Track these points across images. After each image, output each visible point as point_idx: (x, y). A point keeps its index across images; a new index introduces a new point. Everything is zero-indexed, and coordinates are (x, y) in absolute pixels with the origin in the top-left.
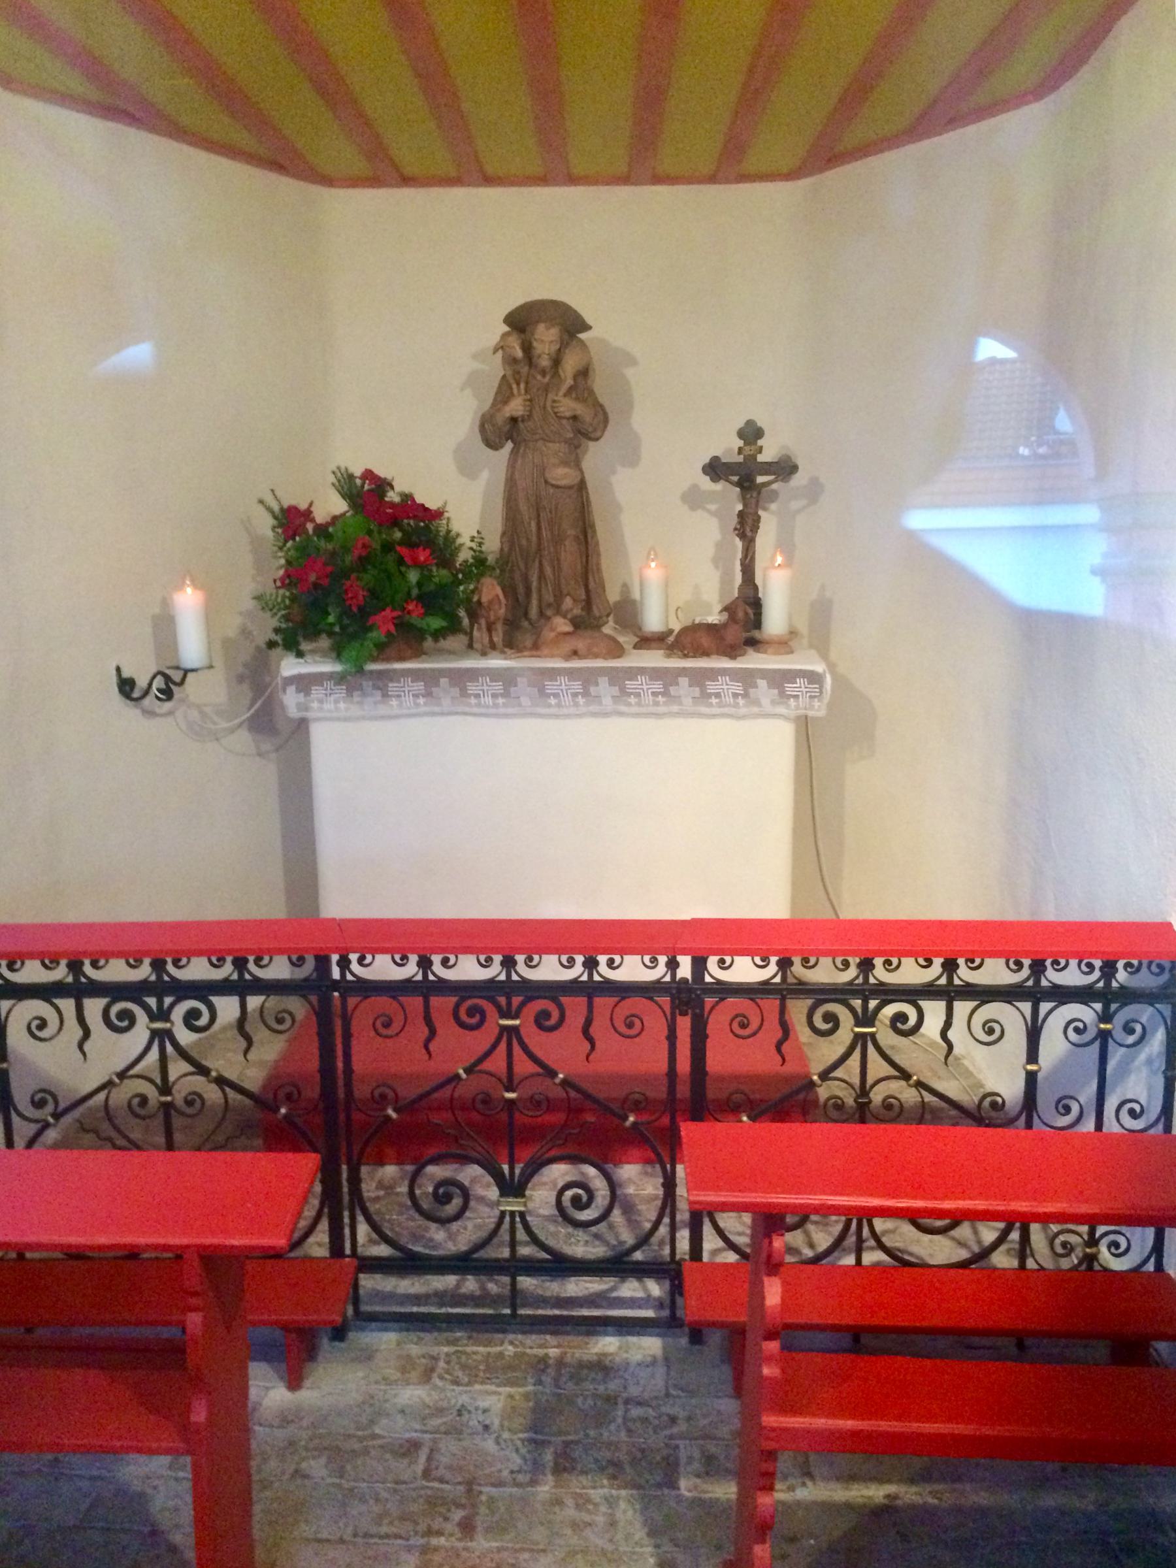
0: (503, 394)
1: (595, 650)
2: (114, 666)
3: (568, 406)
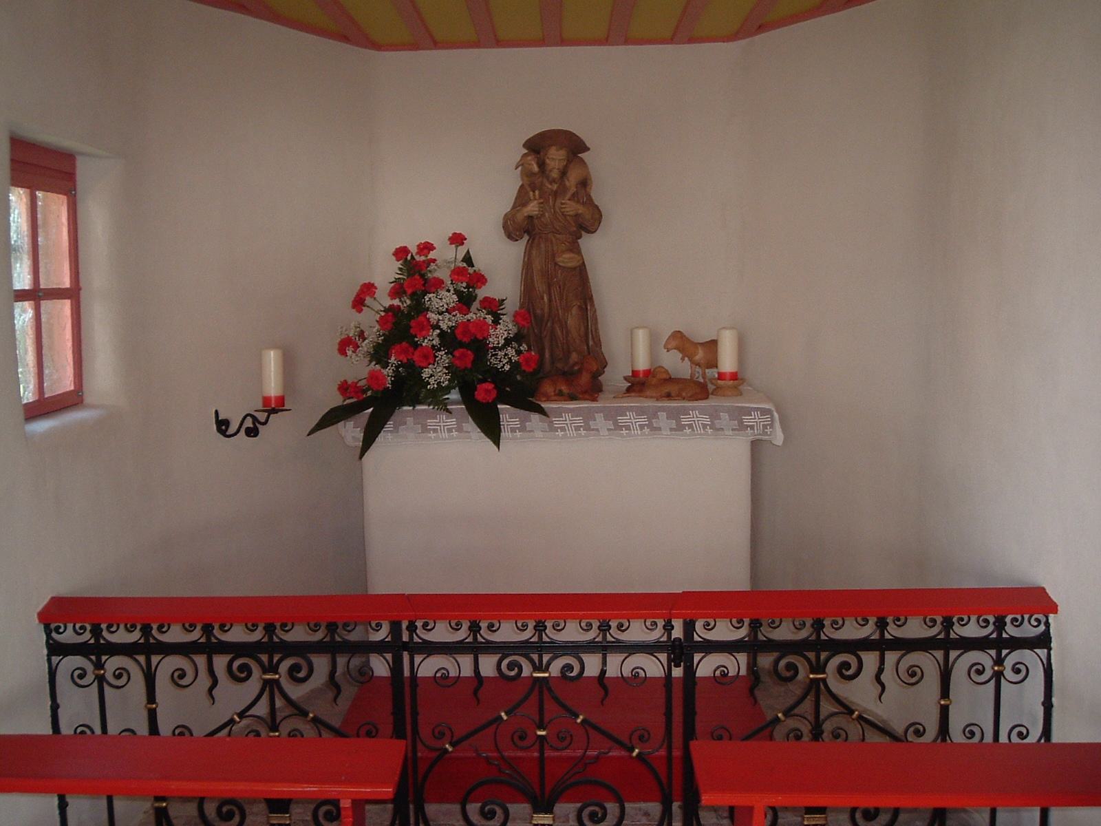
0: (521, 200)
1: (684, 394)
2: (214, 411)
3: (571, 208)
